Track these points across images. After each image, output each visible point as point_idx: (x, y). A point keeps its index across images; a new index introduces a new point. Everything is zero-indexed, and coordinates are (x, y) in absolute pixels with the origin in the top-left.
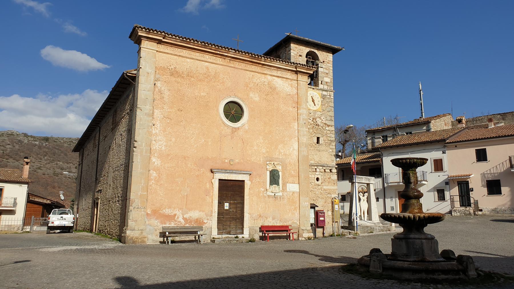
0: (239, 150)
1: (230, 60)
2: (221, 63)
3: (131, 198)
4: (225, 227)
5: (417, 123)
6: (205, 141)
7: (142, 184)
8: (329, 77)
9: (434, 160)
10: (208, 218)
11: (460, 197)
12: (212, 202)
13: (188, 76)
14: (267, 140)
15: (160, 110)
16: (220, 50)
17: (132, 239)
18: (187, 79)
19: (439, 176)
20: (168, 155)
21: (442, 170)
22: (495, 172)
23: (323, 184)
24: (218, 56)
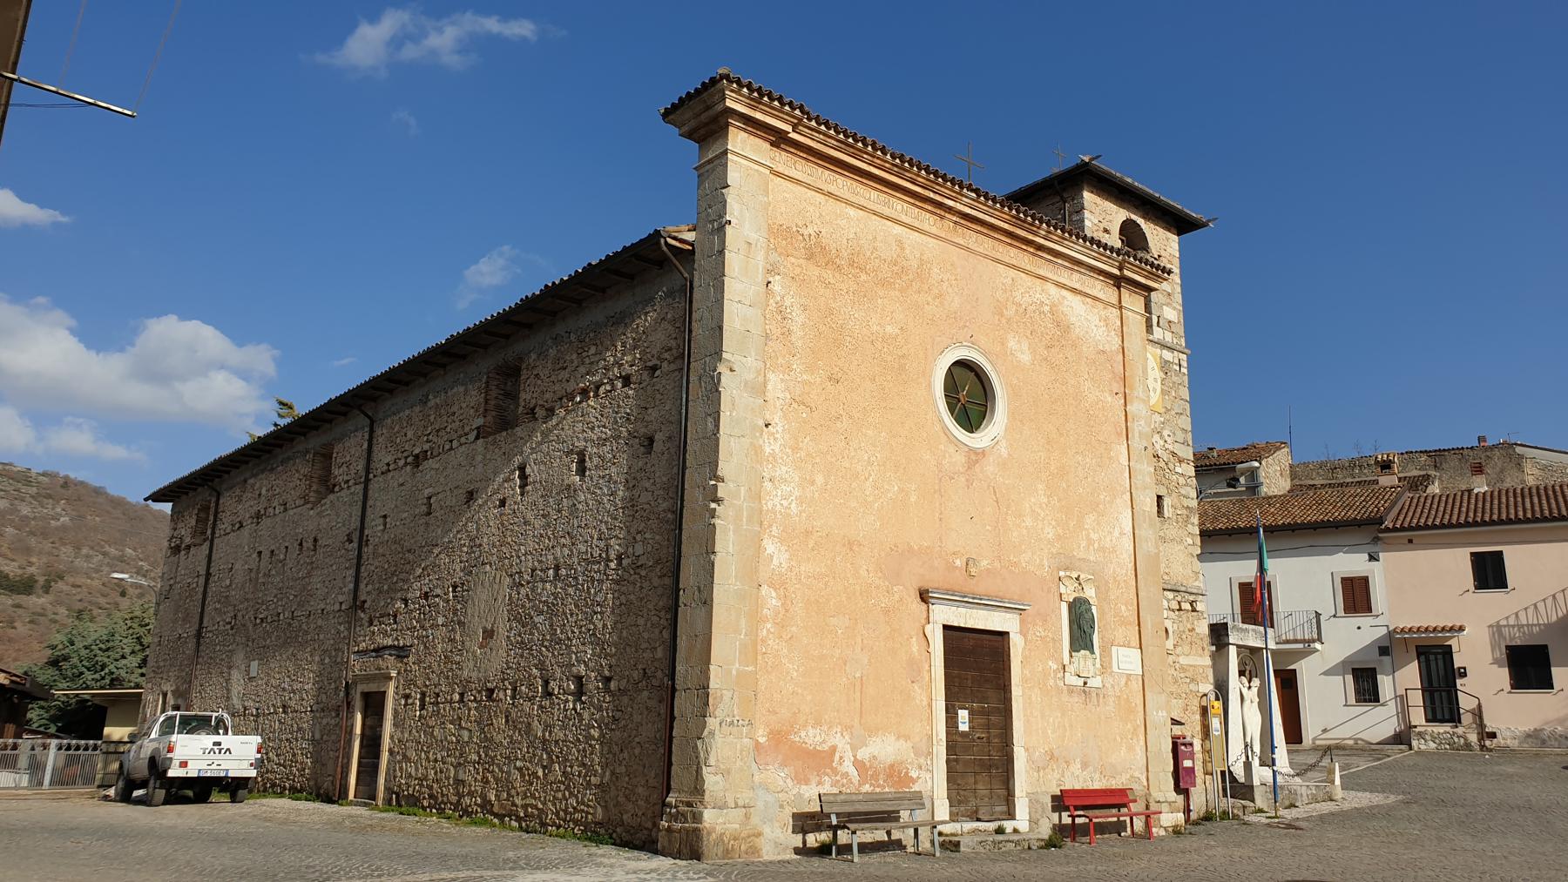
0: (988, 527)
1: (955, 223)
2: (934, 230)
3: (711, 686)
4: (964, 796)
5: (1220, 465)
6: (901, 490)
7: (742, 637)
9: (1343, 580)
10: (922, 761)
11: (1427, 694)
13: (852, 264)
14: (1055, 498)
15: (781, 376)
16: (937, 187)
17: (722, 840)
18: (850, 276)
19: (1359, 628)
20: (808, 533)
21: (1370, 610)
22: (1530, 623)
23: (1179, 650)
24: (926, 206)
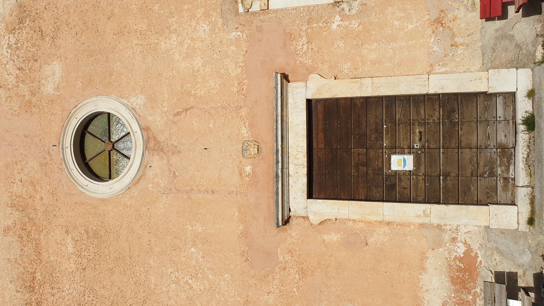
4: (485, 166)
10: (447, 237)
12: (389, 223)
14: (170, 20)
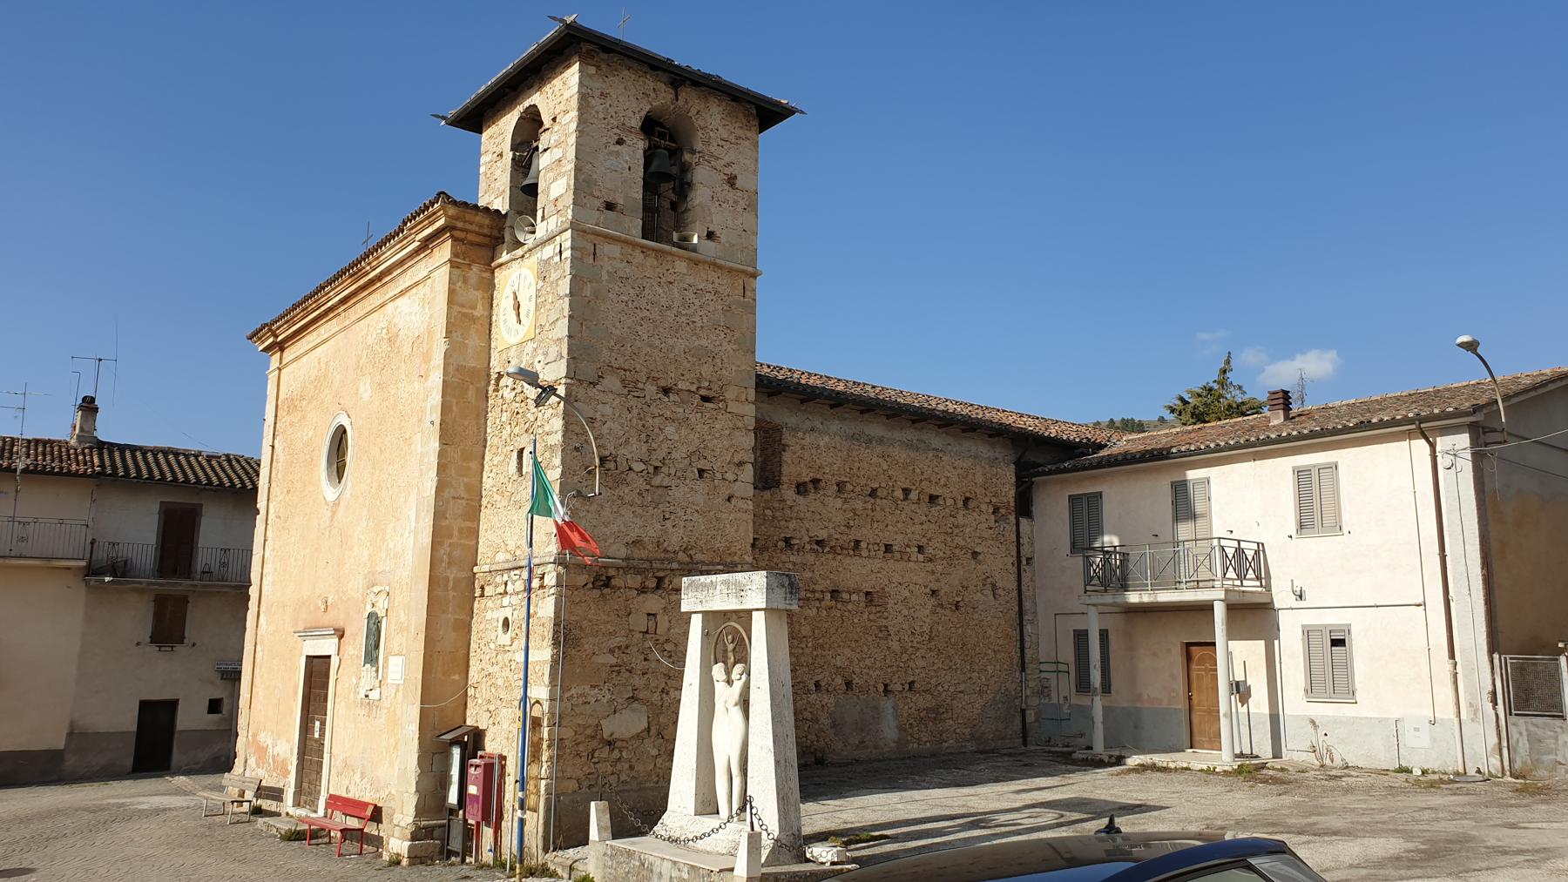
8: (563, 170)
